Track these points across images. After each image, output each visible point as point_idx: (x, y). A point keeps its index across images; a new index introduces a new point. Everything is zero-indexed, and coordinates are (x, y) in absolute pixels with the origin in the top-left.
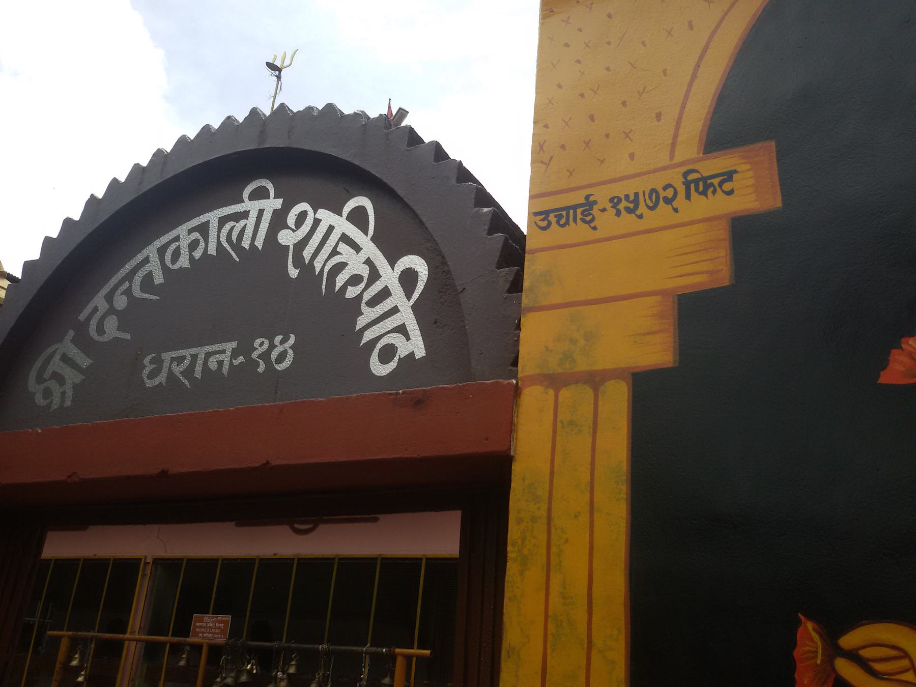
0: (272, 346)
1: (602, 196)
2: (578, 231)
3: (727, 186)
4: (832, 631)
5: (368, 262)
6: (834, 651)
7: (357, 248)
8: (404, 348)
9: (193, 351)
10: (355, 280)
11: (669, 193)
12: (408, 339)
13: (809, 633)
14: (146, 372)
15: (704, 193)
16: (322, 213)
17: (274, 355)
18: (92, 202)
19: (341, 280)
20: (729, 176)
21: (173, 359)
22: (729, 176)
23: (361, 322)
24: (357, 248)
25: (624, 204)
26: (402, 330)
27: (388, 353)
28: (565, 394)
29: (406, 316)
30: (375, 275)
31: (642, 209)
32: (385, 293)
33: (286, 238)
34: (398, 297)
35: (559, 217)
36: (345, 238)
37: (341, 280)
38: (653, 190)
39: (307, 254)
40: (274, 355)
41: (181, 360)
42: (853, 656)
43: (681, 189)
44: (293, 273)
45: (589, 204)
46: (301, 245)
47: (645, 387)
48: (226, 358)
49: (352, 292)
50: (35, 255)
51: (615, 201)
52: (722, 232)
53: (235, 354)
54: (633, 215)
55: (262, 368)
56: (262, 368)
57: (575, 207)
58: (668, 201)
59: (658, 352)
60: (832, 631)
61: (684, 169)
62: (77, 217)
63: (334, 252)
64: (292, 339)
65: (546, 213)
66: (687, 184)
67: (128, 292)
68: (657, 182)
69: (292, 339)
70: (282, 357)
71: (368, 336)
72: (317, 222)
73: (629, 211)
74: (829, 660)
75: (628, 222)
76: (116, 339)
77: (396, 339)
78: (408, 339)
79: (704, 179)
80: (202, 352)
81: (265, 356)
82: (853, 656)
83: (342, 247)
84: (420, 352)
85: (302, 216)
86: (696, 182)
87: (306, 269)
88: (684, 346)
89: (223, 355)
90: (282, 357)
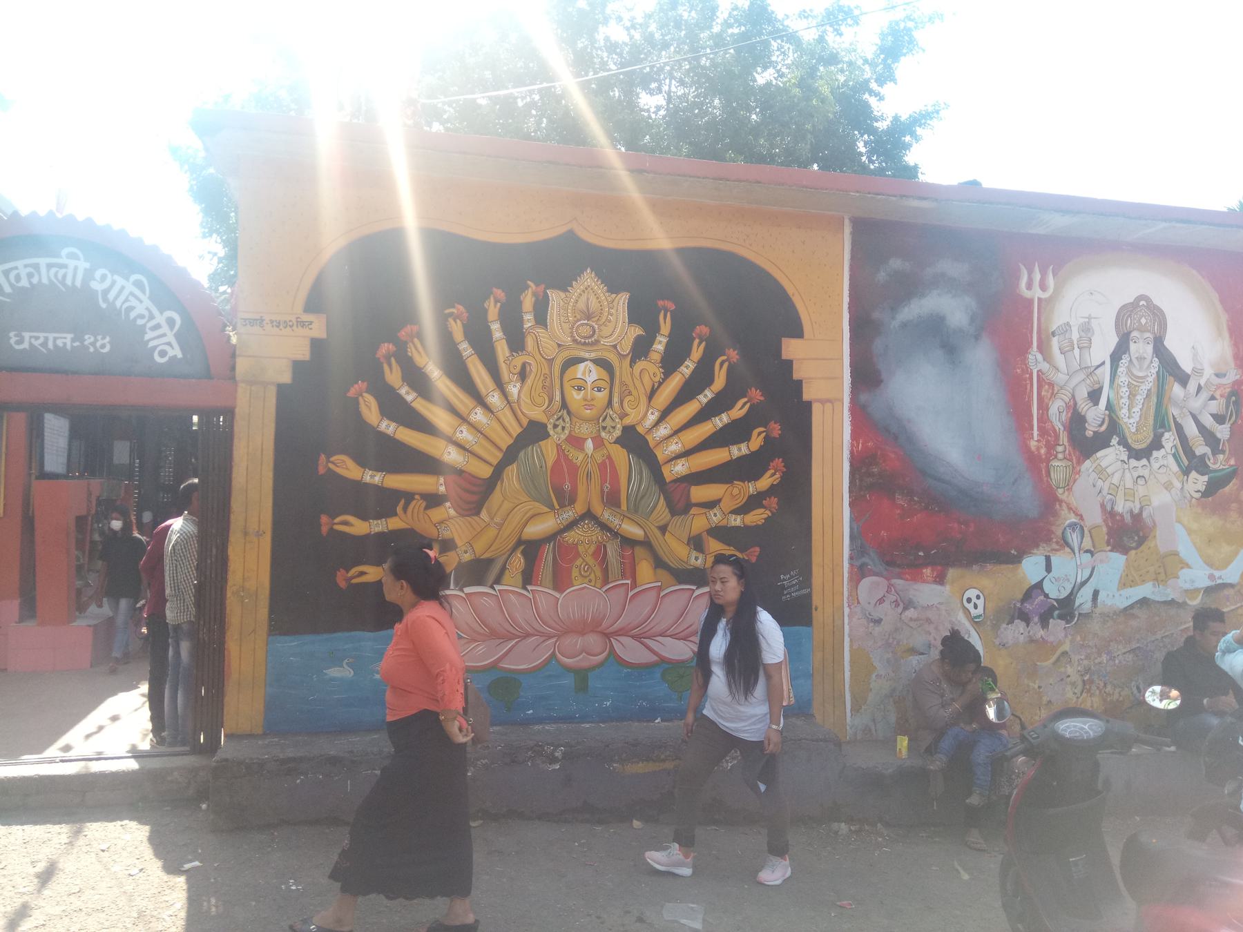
0: (96, 340)
4: (328, 458)
5: (147, 309)
7: (141, 302)
8: (171, 353)
16: (116, 277)
17: (98, 344)
18: (89, 221)
20: (311, 323)
22: (311, 323)
23: (147, 337)
24: (141, 302)
26: (169, 344)
29: (170, 337)
32: (158, 327)
33: (95, 285)
34: (165, 329)
36: (132, 294)
40: (98, 344)
47: (281, 388)
48: (68, 342)
49: (140, 322)
50: (80, 218)
51: (272, 322)
52: (308, 342)
53: (73, 340)
54: (694, 511)
56: (92, 350)
60: (328, 458)
62: (922, 178)
63: (126, 300)
64: (108, 339)
69: (108, 339)
70: (103, 346)
72: (114, 283)
77: (167, 348)
80: (51, 336)
81: (93, 344)
83: (131, 298)
85: (104, 277)
88: (294, 378)
89: (66, 340)
90: (103, 346)
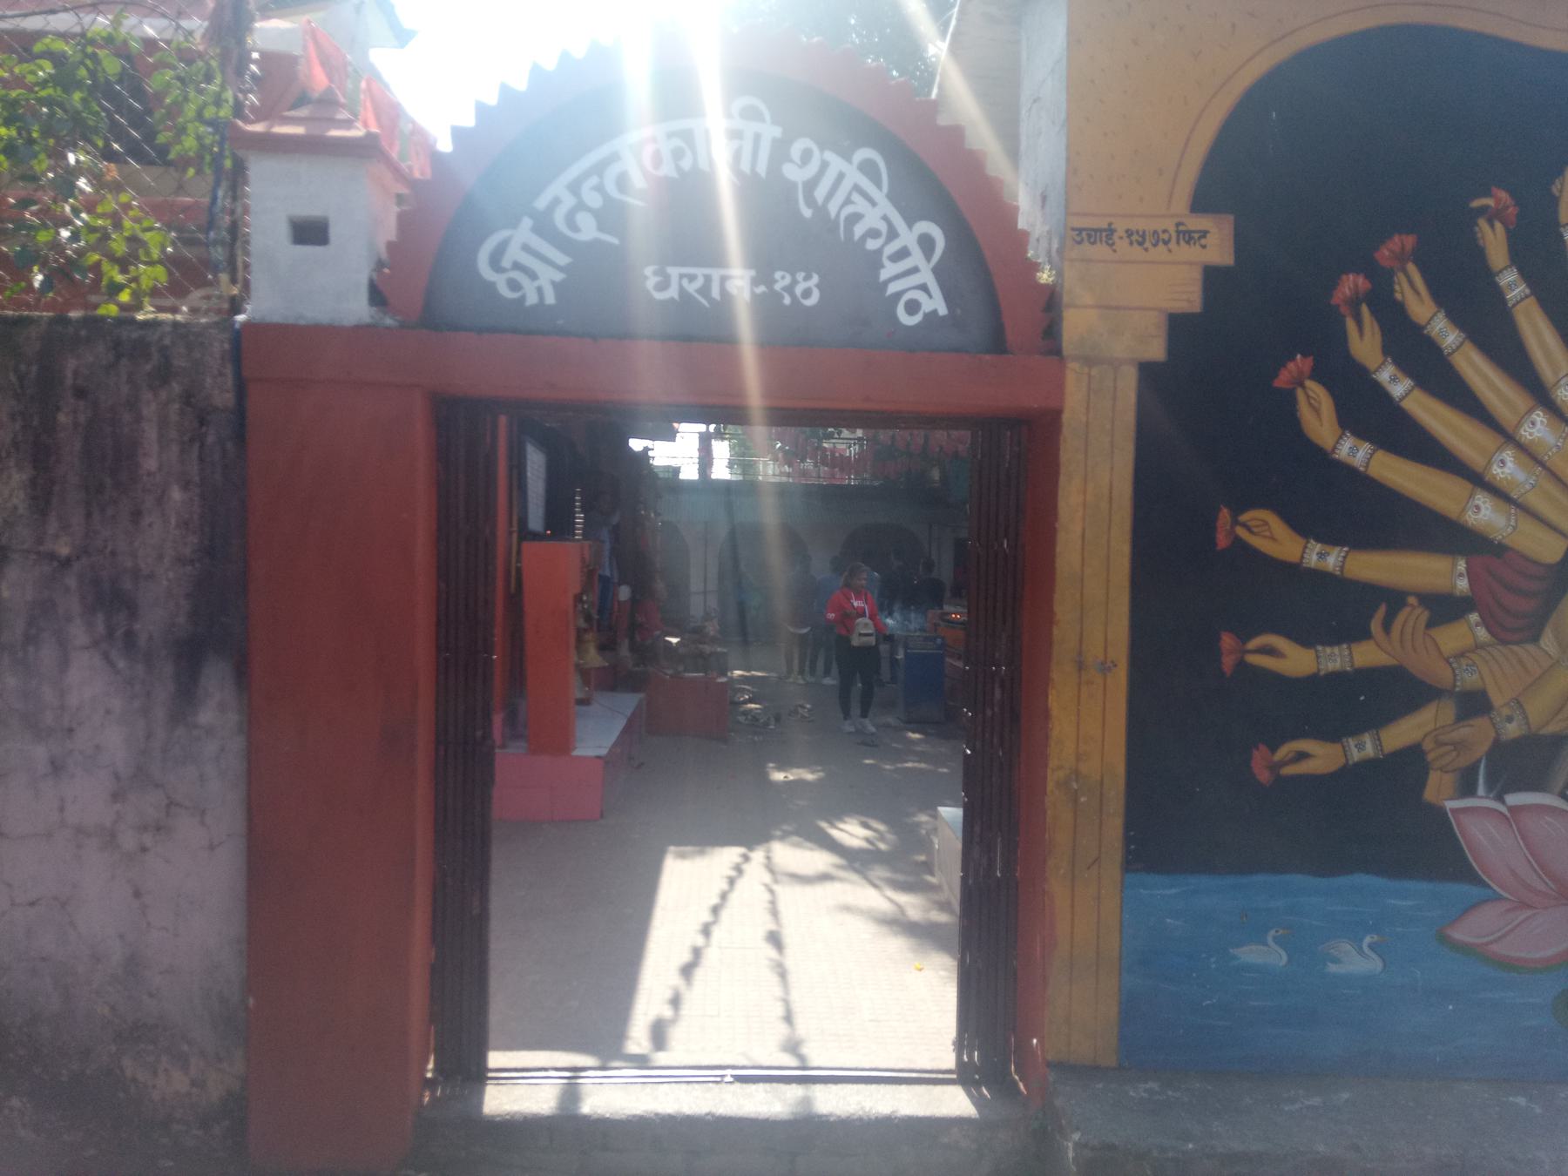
0: (795, 282)
1: (1121, 227)
2: (1100, 250)
3: (1203, 241)
5: (885, 218)
6: (1235, 522)
7: (873, 203)
8: (928, 305)
9: (707, 271)
10: (874, 233)
11: (1166, 236)
12: (930, 296)
13: (1225, 514)
14: (651, 282)
15: (1188, 242)
17: (799, 290)
19: (859, 230)
20: (1204, 234)
21: (681, 276)
22: (1204, 234)
23: (884, 275)
24: (873, 203)
25: (1135, 237)
26: (924, 288)
27: (913, 307)
28: (1094, 372)
30: (893, 234)
31: (1147, 244)
32: (903, 254)
34: (917, 258)
35: (1089, 236)
36: (857, 188)
37: (859, 230)
38: (1155, 232)
39: (820, 193)
41: (692, 278)
42: (1244, 525)
43: (1174, 235)
44: (807, 213)
45: (1110, 231)
46: (811, 185)
47: (1148, 371)
49: (872, 245)
51: (1129, 233)
52: (1197, 275)
55: (787, 301)
57: (1101, 230)
58: (1166, 243)
59: (1156, 351)
61: (1176, 220)
65: (1080, 231)
66: (1178, 232)
67: (599, 188)
68: (1159, 225)
69: (815, 279)
70: (807, 293)
71: (893, 288)
72: (824, 166)
73: (1140, 244)
74: (1232, 527)
75: (1137, 252)
76: (596, 243)
77: (919, 295)
78: (930, 296)
79: (1190, 232)
81: (790, 289)
82: (1244, 525)
83: (856, 197)
84: (943, 310)
86: (1184, 232)
87: (821, 211)
90: (807, 293)
